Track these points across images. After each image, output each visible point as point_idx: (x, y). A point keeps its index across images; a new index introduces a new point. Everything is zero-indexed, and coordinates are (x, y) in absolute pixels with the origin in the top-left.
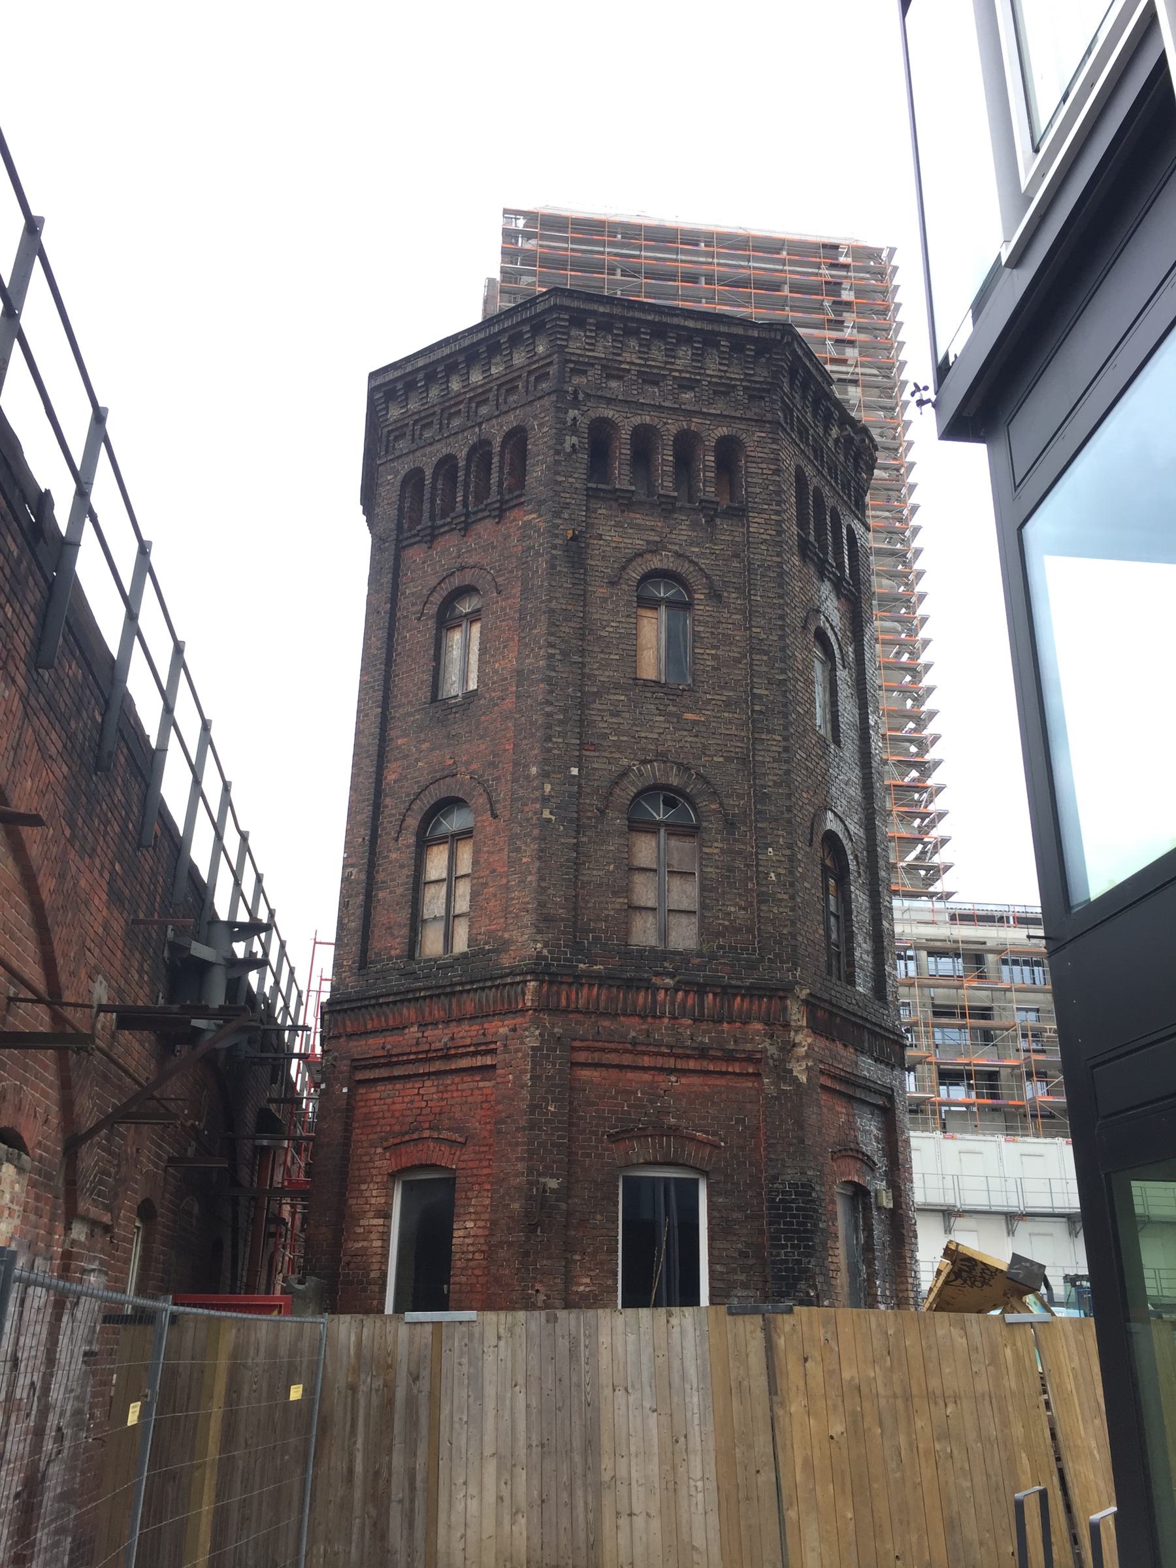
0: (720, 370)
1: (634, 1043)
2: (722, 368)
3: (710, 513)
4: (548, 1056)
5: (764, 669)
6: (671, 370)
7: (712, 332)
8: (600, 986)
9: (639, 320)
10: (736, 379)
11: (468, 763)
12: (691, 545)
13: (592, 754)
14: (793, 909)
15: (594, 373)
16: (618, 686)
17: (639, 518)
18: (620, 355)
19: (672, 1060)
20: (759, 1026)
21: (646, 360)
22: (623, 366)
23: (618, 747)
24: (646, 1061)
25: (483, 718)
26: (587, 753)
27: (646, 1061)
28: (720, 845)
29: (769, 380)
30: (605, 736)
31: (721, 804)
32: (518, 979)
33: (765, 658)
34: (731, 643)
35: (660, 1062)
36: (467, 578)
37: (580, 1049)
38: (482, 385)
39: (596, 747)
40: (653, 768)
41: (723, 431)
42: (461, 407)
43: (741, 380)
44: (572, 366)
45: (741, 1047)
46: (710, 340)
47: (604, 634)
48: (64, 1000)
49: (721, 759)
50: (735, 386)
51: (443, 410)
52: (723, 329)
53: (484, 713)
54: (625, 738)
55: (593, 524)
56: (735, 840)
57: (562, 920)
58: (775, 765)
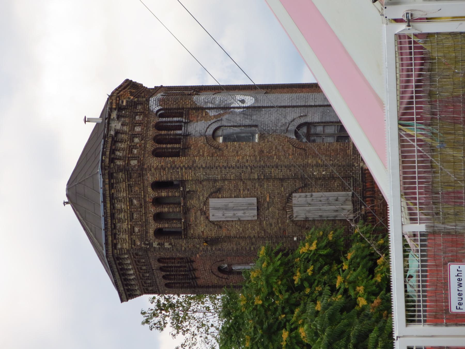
0: (124, 191)
2: (122, 191)
3: (186, 195)
7: (110, 197)
9: (111, 224)
10: (126, 184)
12: (199, 199)
15: (134, 237)
17: (192, 219)
18: (126, 229)
21: (125, 220)
23: (283, 223)
26: (287, 234)
29: (123, 172)
30: (280, 228)
31: (299, 188)
33: (242, 174)
34: (237, 185)
39: (284, 231)
40: (289, 212)
41: (150, 189)
44: (133, 246)
46: (112, 197)
47: (241, 229)
48: (200, 282)
49: (282, 188)
50: (128, 185)
51: (141, 279)
52: (108, 192)
54: (280, 221)
55: (199, 235)
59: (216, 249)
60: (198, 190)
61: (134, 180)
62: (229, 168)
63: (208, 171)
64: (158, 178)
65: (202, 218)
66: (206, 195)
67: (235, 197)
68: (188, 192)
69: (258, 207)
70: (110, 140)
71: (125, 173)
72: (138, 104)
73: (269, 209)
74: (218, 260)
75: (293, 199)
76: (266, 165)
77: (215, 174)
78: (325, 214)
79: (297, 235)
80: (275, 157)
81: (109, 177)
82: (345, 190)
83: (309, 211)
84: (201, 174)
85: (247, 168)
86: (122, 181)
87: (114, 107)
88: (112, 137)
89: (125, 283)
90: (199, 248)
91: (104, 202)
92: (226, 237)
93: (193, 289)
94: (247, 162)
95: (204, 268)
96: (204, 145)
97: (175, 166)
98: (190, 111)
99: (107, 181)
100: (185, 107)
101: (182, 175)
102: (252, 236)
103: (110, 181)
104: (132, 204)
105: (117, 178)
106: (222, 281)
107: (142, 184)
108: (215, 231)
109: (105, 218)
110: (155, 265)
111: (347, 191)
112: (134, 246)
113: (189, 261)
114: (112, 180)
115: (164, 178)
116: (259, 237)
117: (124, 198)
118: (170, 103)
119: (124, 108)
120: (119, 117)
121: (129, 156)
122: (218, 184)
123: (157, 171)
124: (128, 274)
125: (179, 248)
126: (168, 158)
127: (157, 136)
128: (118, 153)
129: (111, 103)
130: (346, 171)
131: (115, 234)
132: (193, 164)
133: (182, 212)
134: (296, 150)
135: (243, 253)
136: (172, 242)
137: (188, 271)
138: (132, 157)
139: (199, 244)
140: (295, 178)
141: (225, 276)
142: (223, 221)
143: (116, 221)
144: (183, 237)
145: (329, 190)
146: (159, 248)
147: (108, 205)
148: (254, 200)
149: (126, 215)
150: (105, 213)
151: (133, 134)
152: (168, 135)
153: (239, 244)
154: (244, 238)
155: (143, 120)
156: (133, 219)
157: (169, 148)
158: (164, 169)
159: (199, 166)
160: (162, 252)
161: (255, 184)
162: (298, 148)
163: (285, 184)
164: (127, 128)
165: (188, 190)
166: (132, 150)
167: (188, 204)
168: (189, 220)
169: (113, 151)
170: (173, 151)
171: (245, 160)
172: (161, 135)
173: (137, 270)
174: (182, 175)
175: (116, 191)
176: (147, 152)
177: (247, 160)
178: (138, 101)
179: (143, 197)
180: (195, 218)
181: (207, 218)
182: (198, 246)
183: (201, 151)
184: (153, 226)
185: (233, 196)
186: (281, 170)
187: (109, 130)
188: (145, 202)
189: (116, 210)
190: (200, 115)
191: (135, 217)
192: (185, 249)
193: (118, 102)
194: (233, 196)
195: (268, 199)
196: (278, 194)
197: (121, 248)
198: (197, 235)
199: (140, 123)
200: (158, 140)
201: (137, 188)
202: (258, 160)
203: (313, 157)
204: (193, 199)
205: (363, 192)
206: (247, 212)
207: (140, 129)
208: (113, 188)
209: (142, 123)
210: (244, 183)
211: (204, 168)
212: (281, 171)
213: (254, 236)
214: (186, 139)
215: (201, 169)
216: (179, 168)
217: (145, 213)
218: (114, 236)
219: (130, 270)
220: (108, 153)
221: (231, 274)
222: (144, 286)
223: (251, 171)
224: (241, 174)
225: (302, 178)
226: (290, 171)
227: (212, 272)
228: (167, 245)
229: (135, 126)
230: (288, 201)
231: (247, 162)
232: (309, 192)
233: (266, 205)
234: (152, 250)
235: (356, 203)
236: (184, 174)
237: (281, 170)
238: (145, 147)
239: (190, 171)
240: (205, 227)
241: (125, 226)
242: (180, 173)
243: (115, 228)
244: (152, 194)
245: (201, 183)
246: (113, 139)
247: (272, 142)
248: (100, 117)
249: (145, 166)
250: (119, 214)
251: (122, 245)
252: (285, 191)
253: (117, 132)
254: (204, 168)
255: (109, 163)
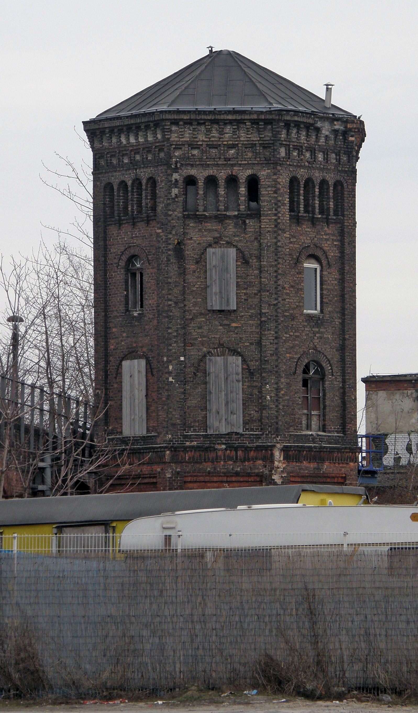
1: (209, 473)
2: (248, 136)
3: (241, 219)
4: (174, 480)
5: (267, 299)
6: (223, 141)
7: (241, 119)
8: (195, 451)
9: (204, 120)
10: (256, 141)
11: (142, 347)
12: (234, 236)
13: (190, 348)
14: (277, 412)
15: (186, 148)
16: (201, 314)
17: (209, 226)
18: (196, 138)
19: (225, 478)
20: (260, 462)
21: (210, 138)
22: (199, 143)
23: (202, 343)
24: (215, 479)
25: (146, 327)
26: (188, 348)
27: (215, 479)
28: (247, 384)
29: (272, 138)
30: (196, 339)
31: (248, 365)
32: (162, 450)
33: (268, 293)
35: (220, 479)
36: (132, 251)
37: (188, 476)
38: (136, 146)
39: (192, 345)
40: (217, 351)
41: (249, 172)
42: (128, 152)
43: (258, 141)
44: (174, 146)
45: (253, 471)
47: (194, 289)
48: (113, 230)
49: (248, 344)
50: (255, 144)
52: (247, 117)
53: (146, 325)
54: (205, 339)
55: (187, 233)
56: (254, 381)
57: (179, 424)
58: (271, 346)
59: (170, 255)
60: (246, 234)
61: (261, 151)
62: (276, 277)
63: (272, 249)
64: (264, 183)
65: (211, 239)
66: (240, 245)
67: (237, 282)
68: (244, 222)
69: (223, 311)
70: (311, 121)
71: (271, 140)
72: (349, 157)
73: (221, 326)
74: (150, 257)
75: (234, 357)
76: (279, 324)
77: (268, 257)
78: (213, 397)
79: (187, 361)
80: (288, 336)
81: (267, 119)
82: (245, 423)
83: (217, 377)
84: (268, 239)
85: (276, 299)
86: (261, 136)
87: (349, 126)
88: (315, 124)
89: (116, 130)
90: (171, 233)
91: (234, 112)
92: (184, 269)
93: (102, 220)
94: (282, 300)
95: (136, 237)
96: (300, 243)
97: (280, 207)
98: (339, 225)
99: (263, 117)
100: (345, 218)
101: (267, 215)
102: (186, 303)
103: (262, 120)
104: (229, 148)
105: (265, 129)
106: (115, 258)
107: (257, 162)
108: (192, 255)
109: (213, 111)
110: (144, 174)
111: (244, 427)
112: (174, 148)
113: (149, 219)
114: (263, 124)
115: (263, 191)
116: (185, 311)
117: (239, 137)
118: (350, 199)
119: (345, 139)
120: (336, 132)
121: (291, 146)
122: (255, 261)
123: (273, 183)
124: (129, 136)
125: (170, 207)
126: (288, 196)
127: (313, 183)
128: (294, 131)
129: (353, 122)
130: (271, 426)
131: (191, 124)
132: (280, 230)
133: (219, 213)
134: (294, 362)
135: (163, 290)
136: (180, 199)
137: (133, 215)
138: (289, 150)
139: (176, 234)
140: (263, 361)
141: (122, 263)
142: (206, 265)
143: (208, 125)
144: (185, 213)
145: (245, 403)
146: (171, 181)
147: (230, 117)
148: (233, 306)
149: (216, 139)
150: (220, 112)
151: (315, 150)
152: (314, 196)
153: (176, 286)
154: (183, 293)
155: (331, 163)
156: (210, 148)
157: (299, 199)
158: (275, 192)
159: (279, 238)
160: (166, 184)
161: (254, 309)
162: (296, 365)
163: (253, 347)
164: (323, 142)
165: (247, 221)
166: (296, 149)
167: (227, 221)
168: (207, 222)
169: (297, 125)
170: (295, 204)
171: (285, 297)
172: (314, 187)
173: (135, 148)
174: (267, 215)
175: (247, 128)
176: (295, 169)
177: (285, 300)
178: (353, 156)
179: (240, 162)
180: (209, 230)
181: (210, 246)
182: (174, 232)
183: (295, 240)
184: (201, 174)
185: (239, 280)
186: (273, 343)
187: (321, 118)
188: (233, 165)
189: (223, 127)
190: (335, 238)
191: (211, 150)
192: (170, 215)
193: (353, 130)
194: (239, 280)
195: (234, 325)
196: (241, 338)
197: (171, 130)
198: (187, 231)
199: (327, 159)
200: (309, 182)
201: (250, 155)
202: (285, 314)
203: (287, 383)
204: (235, 227)
205: (243, 447)
206: (218, 297)
207: (320, 159)
208: (252, 123)
209: (327, 162)
210: (256, 294)
211: (276, 244)
212: (271, 343)
213: (185, 306)
214: (308, 220)
215: (275, 241)
216: (276, 212)
217: (218, 164)
218: (189, 123)
219: (137, 139)
220: (296, 118)
221: (125, 271)
222: (107, 154)
223: (272, 305)
224: (268, 291)
225: (261, 370)
226: (271, 354)
227: (130, 247)
228: (175, 191)
229: (324, 152)
230: (232, 351)
231: (282, 300)
232: (243, 377)
233: (226, 322)
234: (169, 172)
235: (229, 438)
236: (269, 218)
237: (273, 343)
238: (300, 167)
239: (273, 226)
240: (198, 242)
241: (201, 137)
242: (269, 212)
243: (199, 124)
244: (243, 175)
245: (256, 239)
246: (312, 125)
247: (303, 331)
248: (332, 105)
249: (279, 168)
250: (217, 130)
251: (176, 132)
252: (244, 347)
253: (318, 130)
254: (276, 244)
255: (284, 120)
